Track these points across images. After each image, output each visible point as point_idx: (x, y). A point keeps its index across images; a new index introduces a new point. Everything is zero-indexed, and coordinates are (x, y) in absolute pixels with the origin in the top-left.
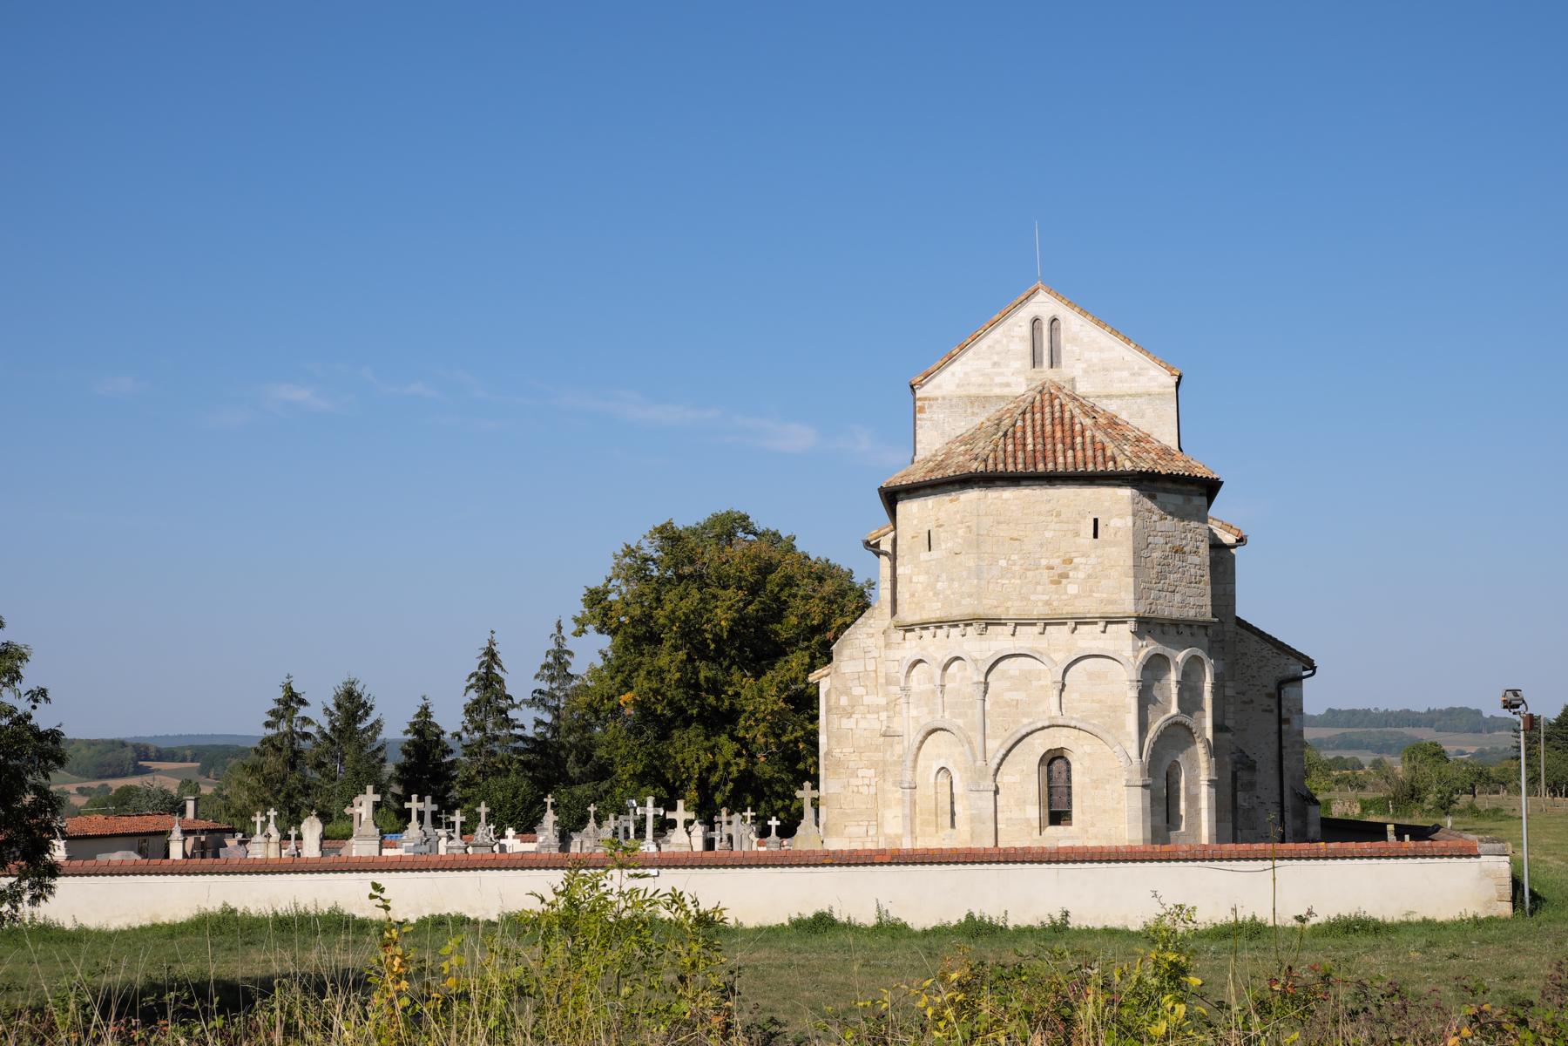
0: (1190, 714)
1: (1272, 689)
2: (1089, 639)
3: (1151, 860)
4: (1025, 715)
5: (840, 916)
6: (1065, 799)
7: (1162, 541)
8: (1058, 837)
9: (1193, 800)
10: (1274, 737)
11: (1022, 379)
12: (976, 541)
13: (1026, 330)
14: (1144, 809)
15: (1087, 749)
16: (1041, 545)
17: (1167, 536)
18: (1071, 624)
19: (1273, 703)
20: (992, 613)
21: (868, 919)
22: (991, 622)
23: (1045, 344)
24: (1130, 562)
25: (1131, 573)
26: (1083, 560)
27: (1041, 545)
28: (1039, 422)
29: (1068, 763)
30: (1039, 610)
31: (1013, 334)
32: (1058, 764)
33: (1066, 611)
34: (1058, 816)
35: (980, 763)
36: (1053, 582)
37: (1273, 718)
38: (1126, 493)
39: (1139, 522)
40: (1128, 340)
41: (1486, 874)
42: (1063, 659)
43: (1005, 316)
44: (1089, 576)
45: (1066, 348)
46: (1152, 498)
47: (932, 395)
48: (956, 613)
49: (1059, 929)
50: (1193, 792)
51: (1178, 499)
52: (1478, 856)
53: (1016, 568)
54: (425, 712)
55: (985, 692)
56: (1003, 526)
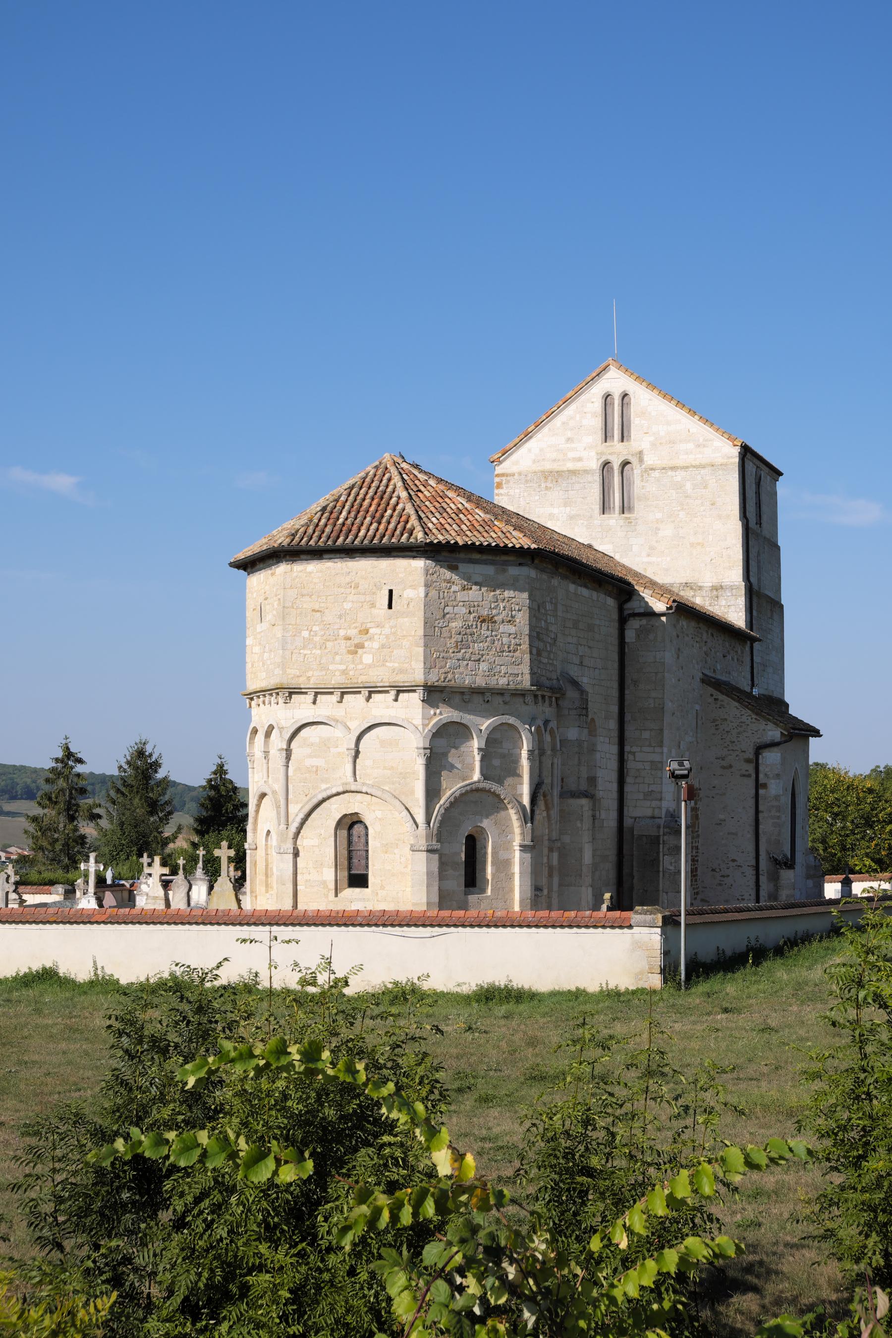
0: (500, 782)
1: (750, 755)
2: (382, 707)
3: (330, 925)
5: (62, 972)
6: (363, 862)
7: (464, 610)
8: (355, 900)
9: (503, 865)
10: (752, 802)
11: (593, 454)
13: (597, 406)
14: (429, 874)
15: (379, 814)
16: (340, 617)
17: (471, 608)
18: (365, 692)
19: (751, 768)
20: (294, 683)
21: (82, 973)
22: (292, 692)
23: (616, 420)
24: (421, 632)
25: (422, 642)
26: (378, 631)
27: (340, 617)
28: (361, 496)
29: (366, 828)
30: (337, 680)
31: (585, 410)
32: (357, 828)
33: (362, 679)
34: (359, 880)
35: (283, 826)
36: (350, 652)
37: (751, 782)
38: (419, 564)
39: (433, 593)
40: (692, 412)
42: (357, 727)
43: (578, 393)
44: (383, 646)
45: (636, 423)
46: (453, 568)
47: (509, 471)
50: (503, 855)
51: (490, 570)
52: (630, 927)
53: (317, 639)
54: (221, 770)
55: (288, 758)
56: (307, 598)
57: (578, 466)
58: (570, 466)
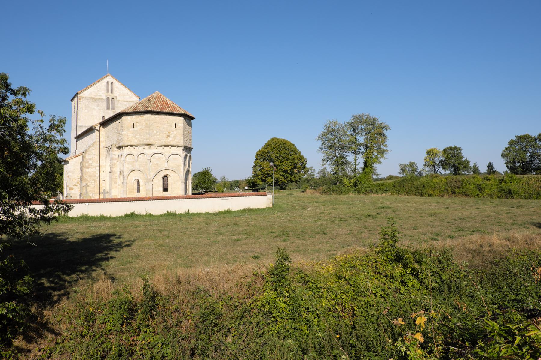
2: (174, 150)
4: (159, 167)
5: (136, 213)
8: (166, 194)
12: (148, 126)
13: (105, 84)
21: (143, 213)
23: (110, 88)
33: (169, 144)
38: (182, 118)
41: (268, 199)
42: (167, 154)
43: (101, 80)
45: (115, 90)
48: (142, 143)
49: (188, 214)
57: (101, 97)
58: (98, 97)
